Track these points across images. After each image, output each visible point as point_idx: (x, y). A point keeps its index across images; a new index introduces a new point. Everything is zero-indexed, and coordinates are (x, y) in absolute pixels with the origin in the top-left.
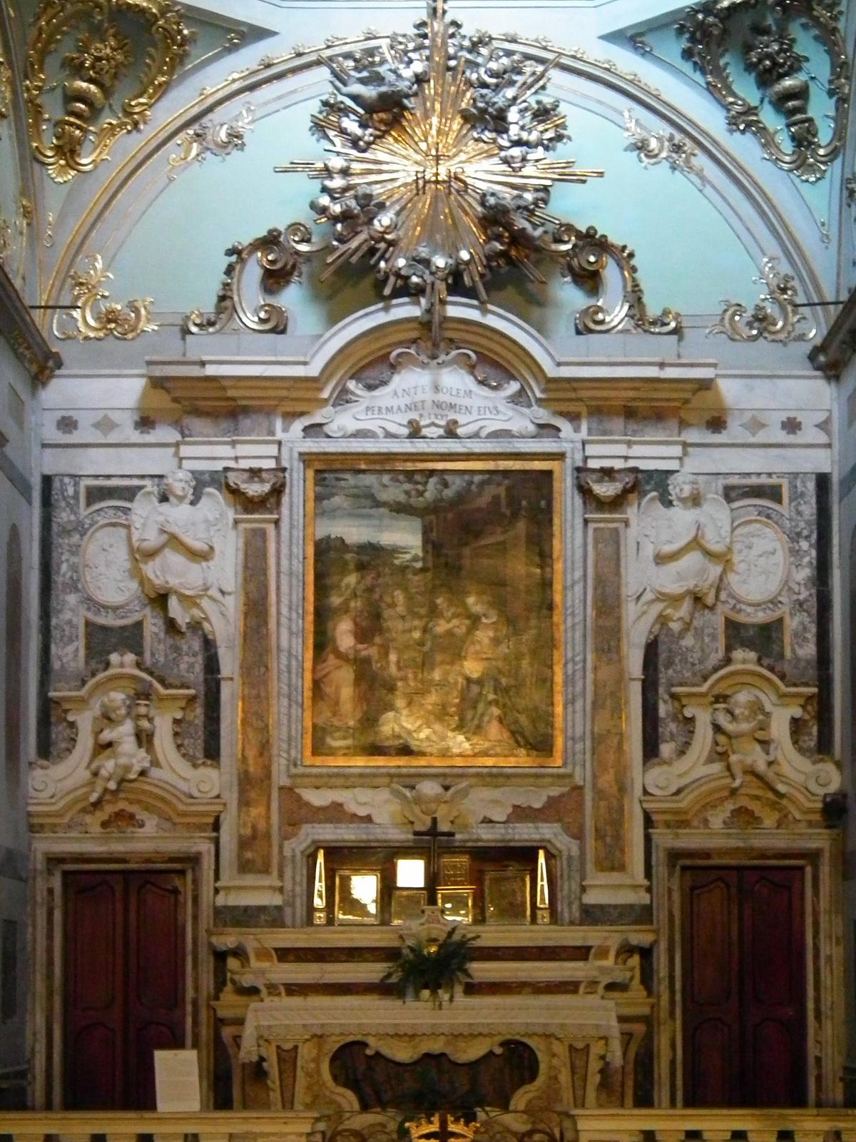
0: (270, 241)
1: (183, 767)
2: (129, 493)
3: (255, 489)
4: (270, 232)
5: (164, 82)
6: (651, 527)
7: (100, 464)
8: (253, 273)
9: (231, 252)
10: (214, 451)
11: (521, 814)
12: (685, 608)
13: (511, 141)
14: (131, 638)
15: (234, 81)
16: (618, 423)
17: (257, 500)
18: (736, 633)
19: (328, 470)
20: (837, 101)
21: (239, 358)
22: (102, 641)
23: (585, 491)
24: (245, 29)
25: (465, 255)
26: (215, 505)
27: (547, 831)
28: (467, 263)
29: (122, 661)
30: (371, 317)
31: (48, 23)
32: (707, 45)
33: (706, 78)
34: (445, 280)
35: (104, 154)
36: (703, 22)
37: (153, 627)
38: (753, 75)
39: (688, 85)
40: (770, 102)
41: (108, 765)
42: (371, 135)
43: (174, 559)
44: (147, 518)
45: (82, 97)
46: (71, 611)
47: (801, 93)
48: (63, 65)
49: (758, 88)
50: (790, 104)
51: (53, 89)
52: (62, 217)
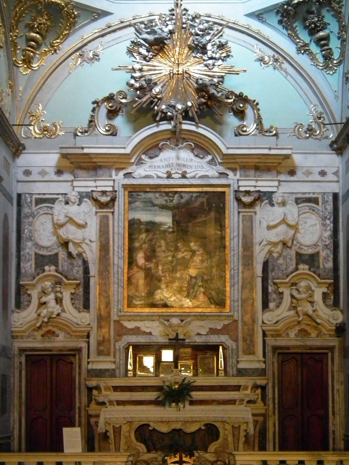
0: (110, 98)
1: (74, 312)
2: (53, 201)
3: (104, 199)
4: (110, 94)
5: (67, 33)
6: (265, 215)
7: (41, 189)
8: (103, 111)
9: (94, 103)
10: (87, 184)
11: (212, 331)
12: (279, 248)
13: (208, 58)
14: (53, 260)
15: (95, 33)
16: (252, 172)
17: (105, 204)
18: (300, 258)
19: (134, 191)
20: (341, 41)
21: (97, 146)
22: (42, 261)
23: (238, 200)
24: (100, 12)
25: (189, 104)
26: (88, 206)
27: (223, 338)
28: (190, 107)
29: (50, 269)
30: (151, 129)
31: (20, 9)
32: (288, 18)
33: (288, 32)
34: (182, 114)
35: (42, 63)
36: (287, 9)
37: (62, 255)
38: (307, 30)
39: (280, 34)
40: (314, 42)
41: (44, 312)
42: (151, 55)
43: (71, 228)
44: (60, 211)
45: (33, 39)
46: (29, 249)
47: (327, 38)
48: (26, 27)
49: (309, 36)
50: (322, 42)
51: (22, 36)
52: (25, 88)
